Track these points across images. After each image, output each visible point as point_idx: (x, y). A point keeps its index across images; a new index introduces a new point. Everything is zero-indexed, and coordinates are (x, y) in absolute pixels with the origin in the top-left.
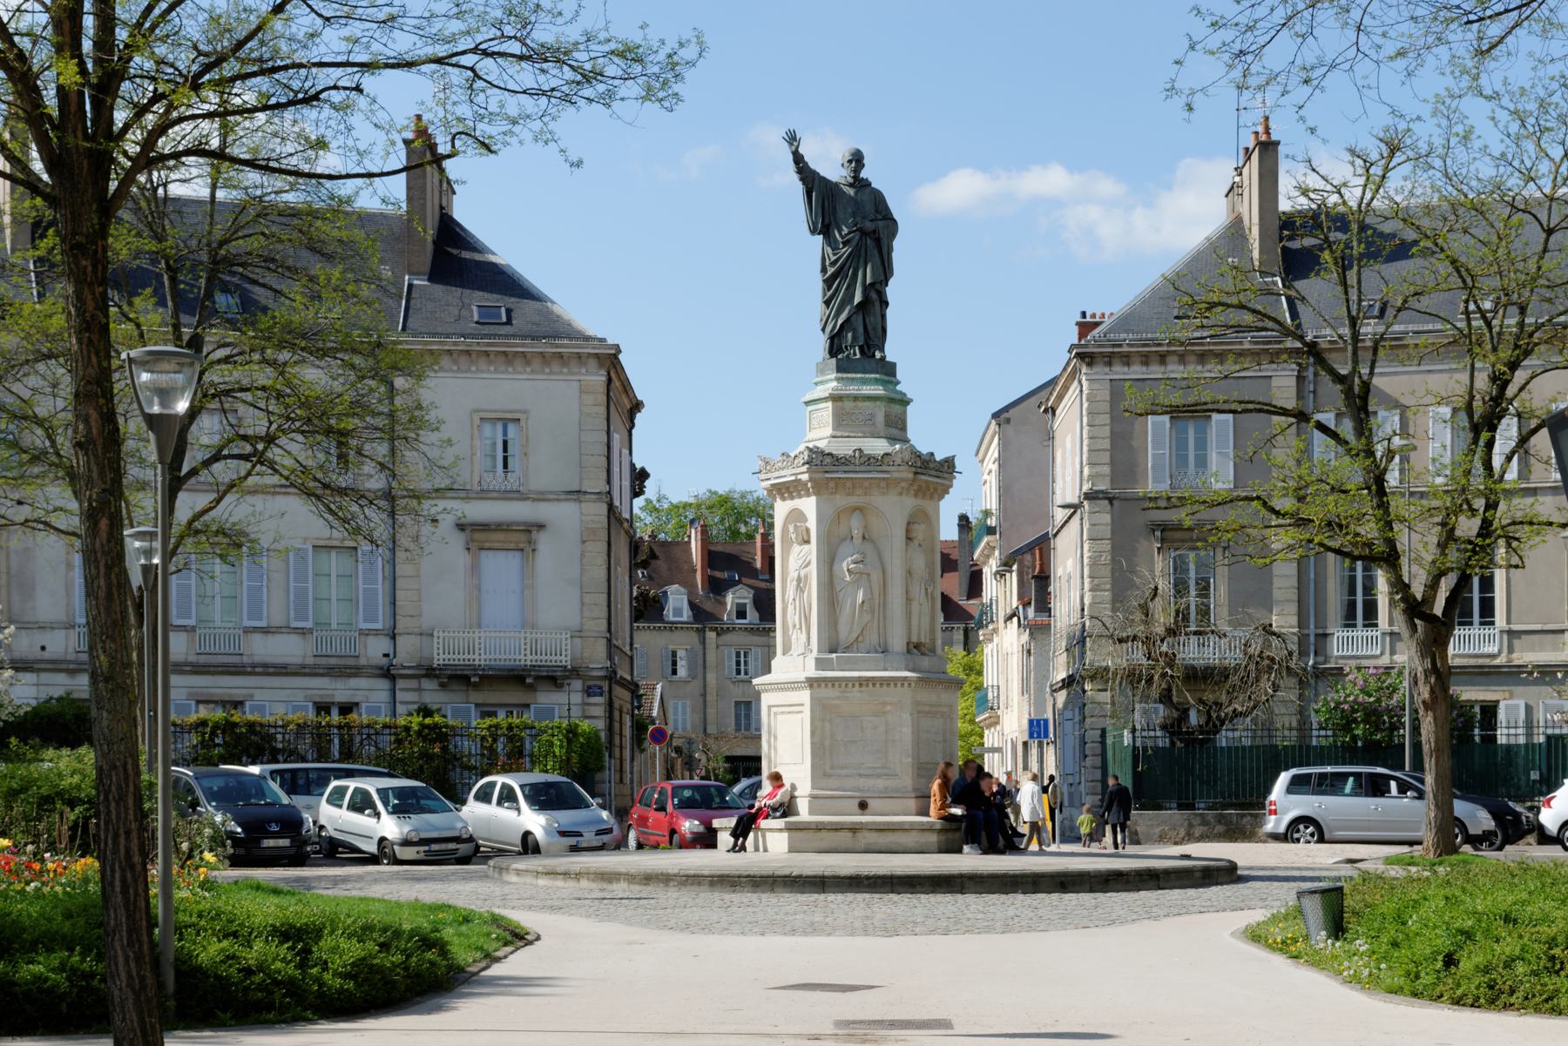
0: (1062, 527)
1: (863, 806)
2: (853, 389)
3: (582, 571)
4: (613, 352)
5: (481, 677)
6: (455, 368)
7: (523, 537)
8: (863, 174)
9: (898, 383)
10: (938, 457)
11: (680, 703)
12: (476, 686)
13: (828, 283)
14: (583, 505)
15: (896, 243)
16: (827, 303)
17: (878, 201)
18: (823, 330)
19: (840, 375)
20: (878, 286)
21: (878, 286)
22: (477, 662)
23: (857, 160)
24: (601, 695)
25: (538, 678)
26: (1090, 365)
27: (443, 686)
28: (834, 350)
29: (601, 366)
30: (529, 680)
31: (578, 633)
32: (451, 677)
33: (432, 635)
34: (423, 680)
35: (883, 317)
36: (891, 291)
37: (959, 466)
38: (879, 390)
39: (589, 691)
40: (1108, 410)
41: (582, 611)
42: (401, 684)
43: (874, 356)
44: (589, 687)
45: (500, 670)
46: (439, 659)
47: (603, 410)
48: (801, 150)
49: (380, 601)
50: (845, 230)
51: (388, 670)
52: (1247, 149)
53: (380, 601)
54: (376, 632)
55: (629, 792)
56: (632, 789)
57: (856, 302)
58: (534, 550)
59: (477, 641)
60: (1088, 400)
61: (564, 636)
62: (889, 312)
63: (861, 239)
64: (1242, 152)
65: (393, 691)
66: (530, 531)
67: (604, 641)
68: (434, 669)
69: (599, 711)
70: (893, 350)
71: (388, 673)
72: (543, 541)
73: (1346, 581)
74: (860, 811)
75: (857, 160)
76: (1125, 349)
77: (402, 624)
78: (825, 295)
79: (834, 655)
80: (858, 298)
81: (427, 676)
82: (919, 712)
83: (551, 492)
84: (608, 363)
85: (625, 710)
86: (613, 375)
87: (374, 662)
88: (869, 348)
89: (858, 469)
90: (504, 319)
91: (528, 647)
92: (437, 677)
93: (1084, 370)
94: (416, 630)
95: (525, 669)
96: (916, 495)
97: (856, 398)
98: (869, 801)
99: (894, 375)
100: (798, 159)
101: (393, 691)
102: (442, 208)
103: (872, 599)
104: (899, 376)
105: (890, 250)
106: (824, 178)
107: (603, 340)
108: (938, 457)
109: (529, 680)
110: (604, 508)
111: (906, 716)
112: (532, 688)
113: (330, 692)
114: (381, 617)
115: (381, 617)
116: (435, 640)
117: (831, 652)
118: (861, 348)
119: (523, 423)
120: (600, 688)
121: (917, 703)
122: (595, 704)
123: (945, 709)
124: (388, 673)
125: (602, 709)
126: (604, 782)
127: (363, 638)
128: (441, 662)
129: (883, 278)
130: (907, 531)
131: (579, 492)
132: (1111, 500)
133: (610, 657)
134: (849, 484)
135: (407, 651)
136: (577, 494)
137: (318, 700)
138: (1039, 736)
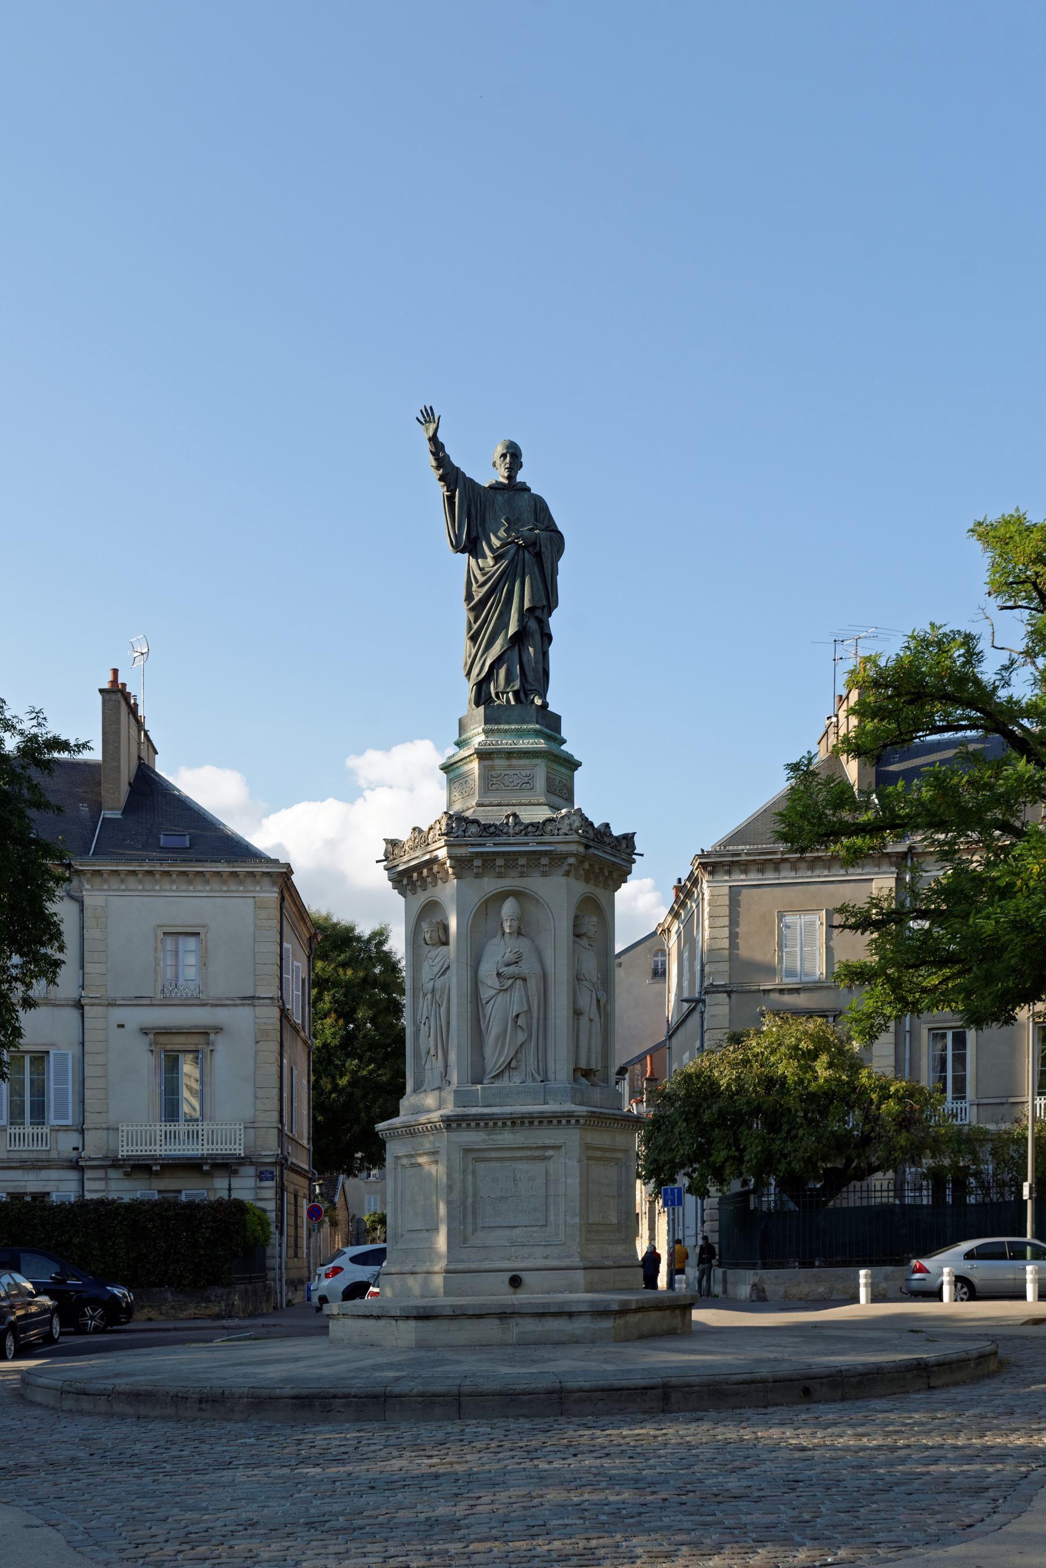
0: (678, 1028)
1: (515, 1282)
2: (506, 743)
3: (256, 1068)
4: (285, 870)
5: (163, 1166)
6: (140, 887)
7: (200, 1039)
8: (520, 477)
9: (564, 742)
10: (616, 831)
11: (373, 1197)
12: (157, 1174)
13: (477, 609)
14: (257, 1009)
15: (562, 564)
16: (474, 638)
17: (540, 509)
18: (468, 674)
19: (489, 727)
20: (538, 613)
21: (538, 613)
22: (158, 1153)
23: (513, 455)
24: (273, 1180)
25: (215, 1166)
26: (711, 873)
27: (127, 1174)
28: (482, 697)
29: (274, 883)
30: (206, 1168)
31: (250, 1125)
32: (134, 1167)
33: (118, 1129)
34: (109, 1170)
35: (545, 655)
36: (556, 622)
37: (640, 845)
38: (541, 744)
39: (261, 1177)
40: (727, 913)
41: (255, 1104)
42: (88, 1174)
43: (533, 701)
44: (262, 1173)
45: (173, 1159)
46: (123, 1152)
47: (275, 923)
48: (441, 437)
49: (70, 1099)
50: (496, 543)
51: (77, 1162)
52: (841, 696)
53: (70, 1099)
54: (66, 1129)
55: (305, 1264)
56: (309, 1262)
57: (511, 633)
58: (212, 1051)
59: (158, 1133)
60: (709, 905)
61: (238, 1127)
62: (552, 650)
63: (517, 553)
64: (837, 699)
65: (82, 1182)
66: (207, 1033)
67: (275, 1131)
68: (119, 1160)
69: (270, 1194)
70: (556, 700)
71: (76, 1165)
72: (222, 1046)
73: (938, 1059)
74: (511, 1290)
75: (513, 455)
76: (743, 858)
77: (91, 1120)
78: (470, 628)
79: (479, 1087)
80: (513, 629)
81: (113, 1166)
82: (589, 1158)
83: (227, 999)
84: (281, 880)
85: (301, 1194)
86: (286, 895)
87: (64, 1155)
88: (526, 696)
89: (512, 840)
90: (188, 845)
91: (205, 1137)
92: (121, 1166)
93: (706, 877)
94: (104, 1126)
95: (202, 1157)
96: (587, 881)
97: (509, 754)
98: (523, 1275)
99: (558, 730)
100: (441, 459)
101: (82, 1182)
102: (140, 758)
103: (529, 1011)
104: (564, 734)
105: (554, 572)
106: (471, 480)
107: (276, 861)
108: (616, 831)
109: (206, 1168)
110: (275, 1012)
111: (574, 1164)
112: (208, 1174)
113: (23, 1183)
114: (70, 1114)
115: (70, 1114)
116: (120, 1133)
117: (474, 1083)
118: (516, 694)
119: (202, 936)
120: (272, 1173)
121: (588, 1147)
122: (266, 1188)
123: (620, 1155)
124: (76, 1165)
125: (273, 1191)
126: (274, 1257)
127: (54, 1134)
128: (125, 1153)
129: (545, 602)
130: (575, 926)
131: (253, 998)
132: (729, 993)
133: (281, 1145)
134: (500, 862)
135: (95, 1146)
136: (251, 1000)
137: (11, 1190)
138: (673, 1204)
